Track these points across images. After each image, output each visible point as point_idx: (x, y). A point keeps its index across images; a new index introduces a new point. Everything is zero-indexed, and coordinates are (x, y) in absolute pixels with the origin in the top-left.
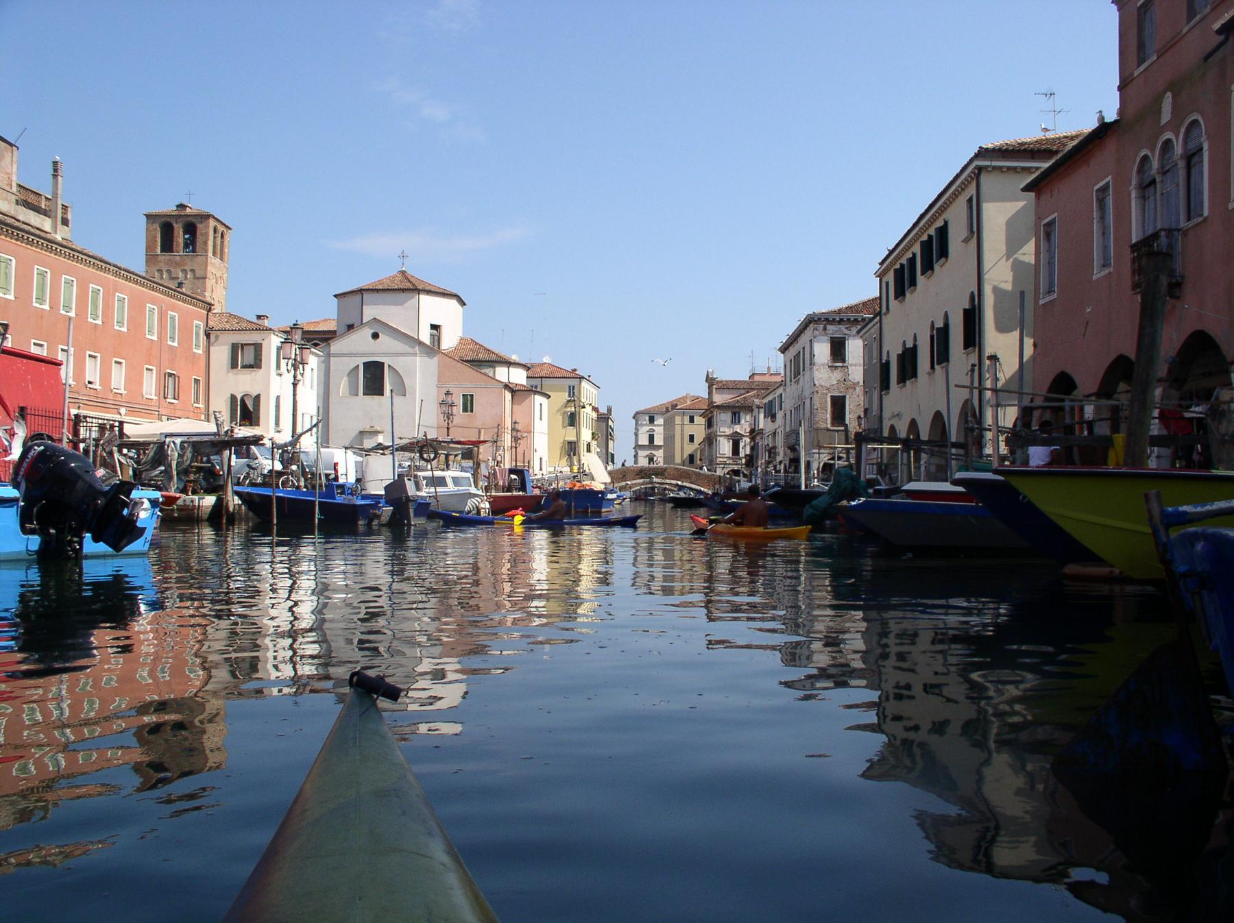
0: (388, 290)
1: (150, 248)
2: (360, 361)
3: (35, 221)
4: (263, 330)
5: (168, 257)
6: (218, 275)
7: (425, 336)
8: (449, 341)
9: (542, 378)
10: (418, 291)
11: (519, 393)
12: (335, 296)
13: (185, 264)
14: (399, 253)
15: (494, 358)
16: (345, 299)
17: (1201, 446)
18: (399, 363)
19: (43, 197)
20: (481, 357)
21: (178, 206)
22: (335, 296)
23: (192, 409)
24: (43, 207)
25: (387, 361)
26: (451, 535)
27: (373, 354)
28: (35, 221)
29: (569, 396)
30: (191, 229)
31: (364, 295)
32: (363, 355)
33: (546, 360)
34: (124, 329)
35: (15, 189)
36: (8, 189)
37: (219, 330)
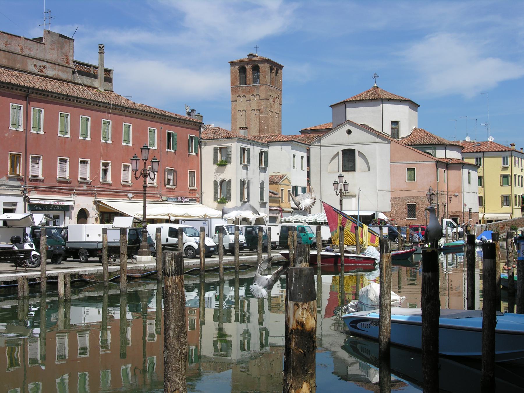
0: (361, 100)
1: (232, 83)
2: (340, 149)
3: (87, 82)
4: (232, 138)
5: (244, 88)
6: (275, 96)
7: (387, 130)
8: (404, 131)
9: (483, 152)
10: (383, 100)
11: (452, 165)
12: (331, 106)
13: (253, 91)
14: (373, 75)
15: (435, 141)
16: (336, 109)
17: (157, 358)
18: (364, 149)
19: (92, 67)
20: (426, 142)
21: (248, 56)
22: (331, 106)
23: (188, 191)
24: (92, 73)
25: (356, 148)
26: (62, 324)
27: (348, 144)
28: (87, 82)
29: (504, 164)
30: (256, 69)
31: (347, 105)
32: (341, 145)
33: (491, 139)
34: (130, 144)
35: (71, 65)
36: (67, 65)
37: (206, 139)
